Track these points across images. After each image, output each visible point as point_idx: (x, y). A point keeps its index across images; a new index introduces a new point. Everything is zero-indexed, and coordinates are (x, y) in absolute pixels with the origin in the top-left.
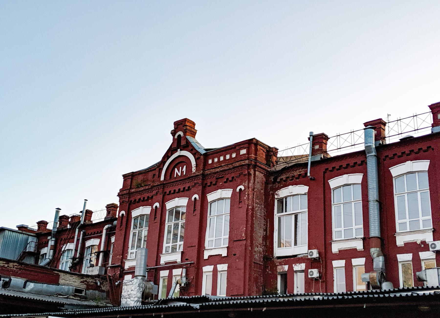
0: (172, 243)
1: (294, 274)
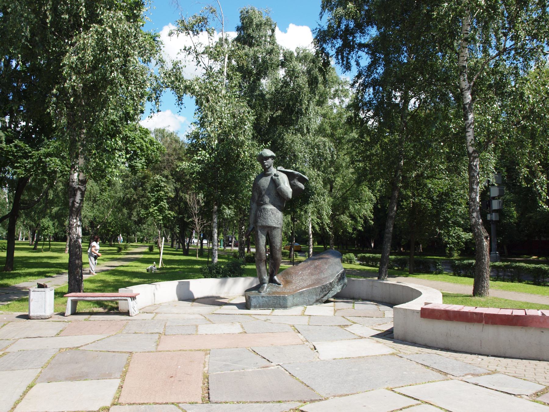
0: (419, 294)
1: (274, 152)
